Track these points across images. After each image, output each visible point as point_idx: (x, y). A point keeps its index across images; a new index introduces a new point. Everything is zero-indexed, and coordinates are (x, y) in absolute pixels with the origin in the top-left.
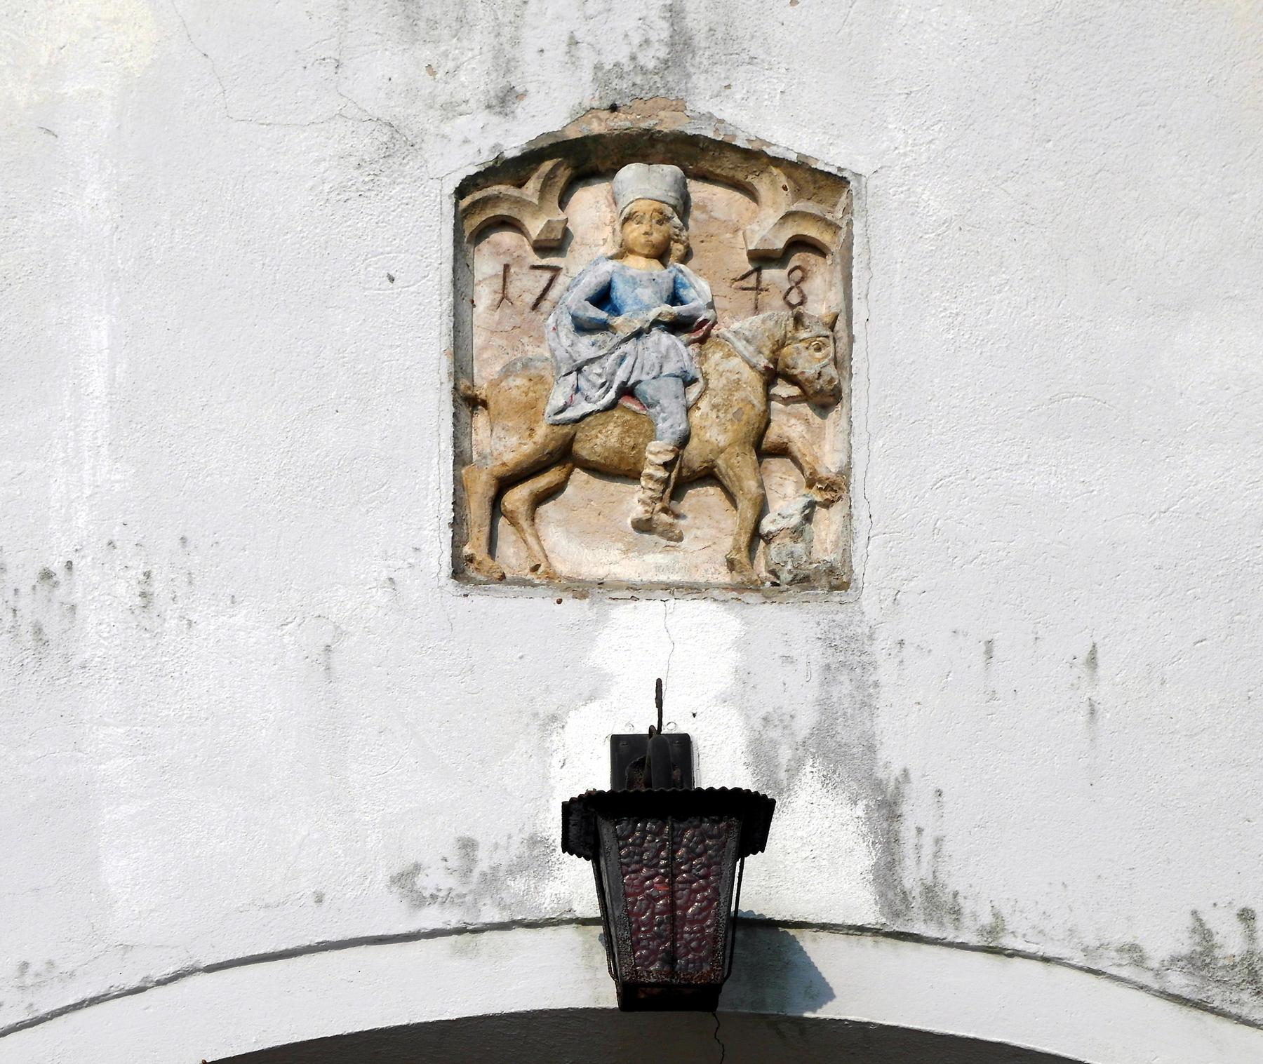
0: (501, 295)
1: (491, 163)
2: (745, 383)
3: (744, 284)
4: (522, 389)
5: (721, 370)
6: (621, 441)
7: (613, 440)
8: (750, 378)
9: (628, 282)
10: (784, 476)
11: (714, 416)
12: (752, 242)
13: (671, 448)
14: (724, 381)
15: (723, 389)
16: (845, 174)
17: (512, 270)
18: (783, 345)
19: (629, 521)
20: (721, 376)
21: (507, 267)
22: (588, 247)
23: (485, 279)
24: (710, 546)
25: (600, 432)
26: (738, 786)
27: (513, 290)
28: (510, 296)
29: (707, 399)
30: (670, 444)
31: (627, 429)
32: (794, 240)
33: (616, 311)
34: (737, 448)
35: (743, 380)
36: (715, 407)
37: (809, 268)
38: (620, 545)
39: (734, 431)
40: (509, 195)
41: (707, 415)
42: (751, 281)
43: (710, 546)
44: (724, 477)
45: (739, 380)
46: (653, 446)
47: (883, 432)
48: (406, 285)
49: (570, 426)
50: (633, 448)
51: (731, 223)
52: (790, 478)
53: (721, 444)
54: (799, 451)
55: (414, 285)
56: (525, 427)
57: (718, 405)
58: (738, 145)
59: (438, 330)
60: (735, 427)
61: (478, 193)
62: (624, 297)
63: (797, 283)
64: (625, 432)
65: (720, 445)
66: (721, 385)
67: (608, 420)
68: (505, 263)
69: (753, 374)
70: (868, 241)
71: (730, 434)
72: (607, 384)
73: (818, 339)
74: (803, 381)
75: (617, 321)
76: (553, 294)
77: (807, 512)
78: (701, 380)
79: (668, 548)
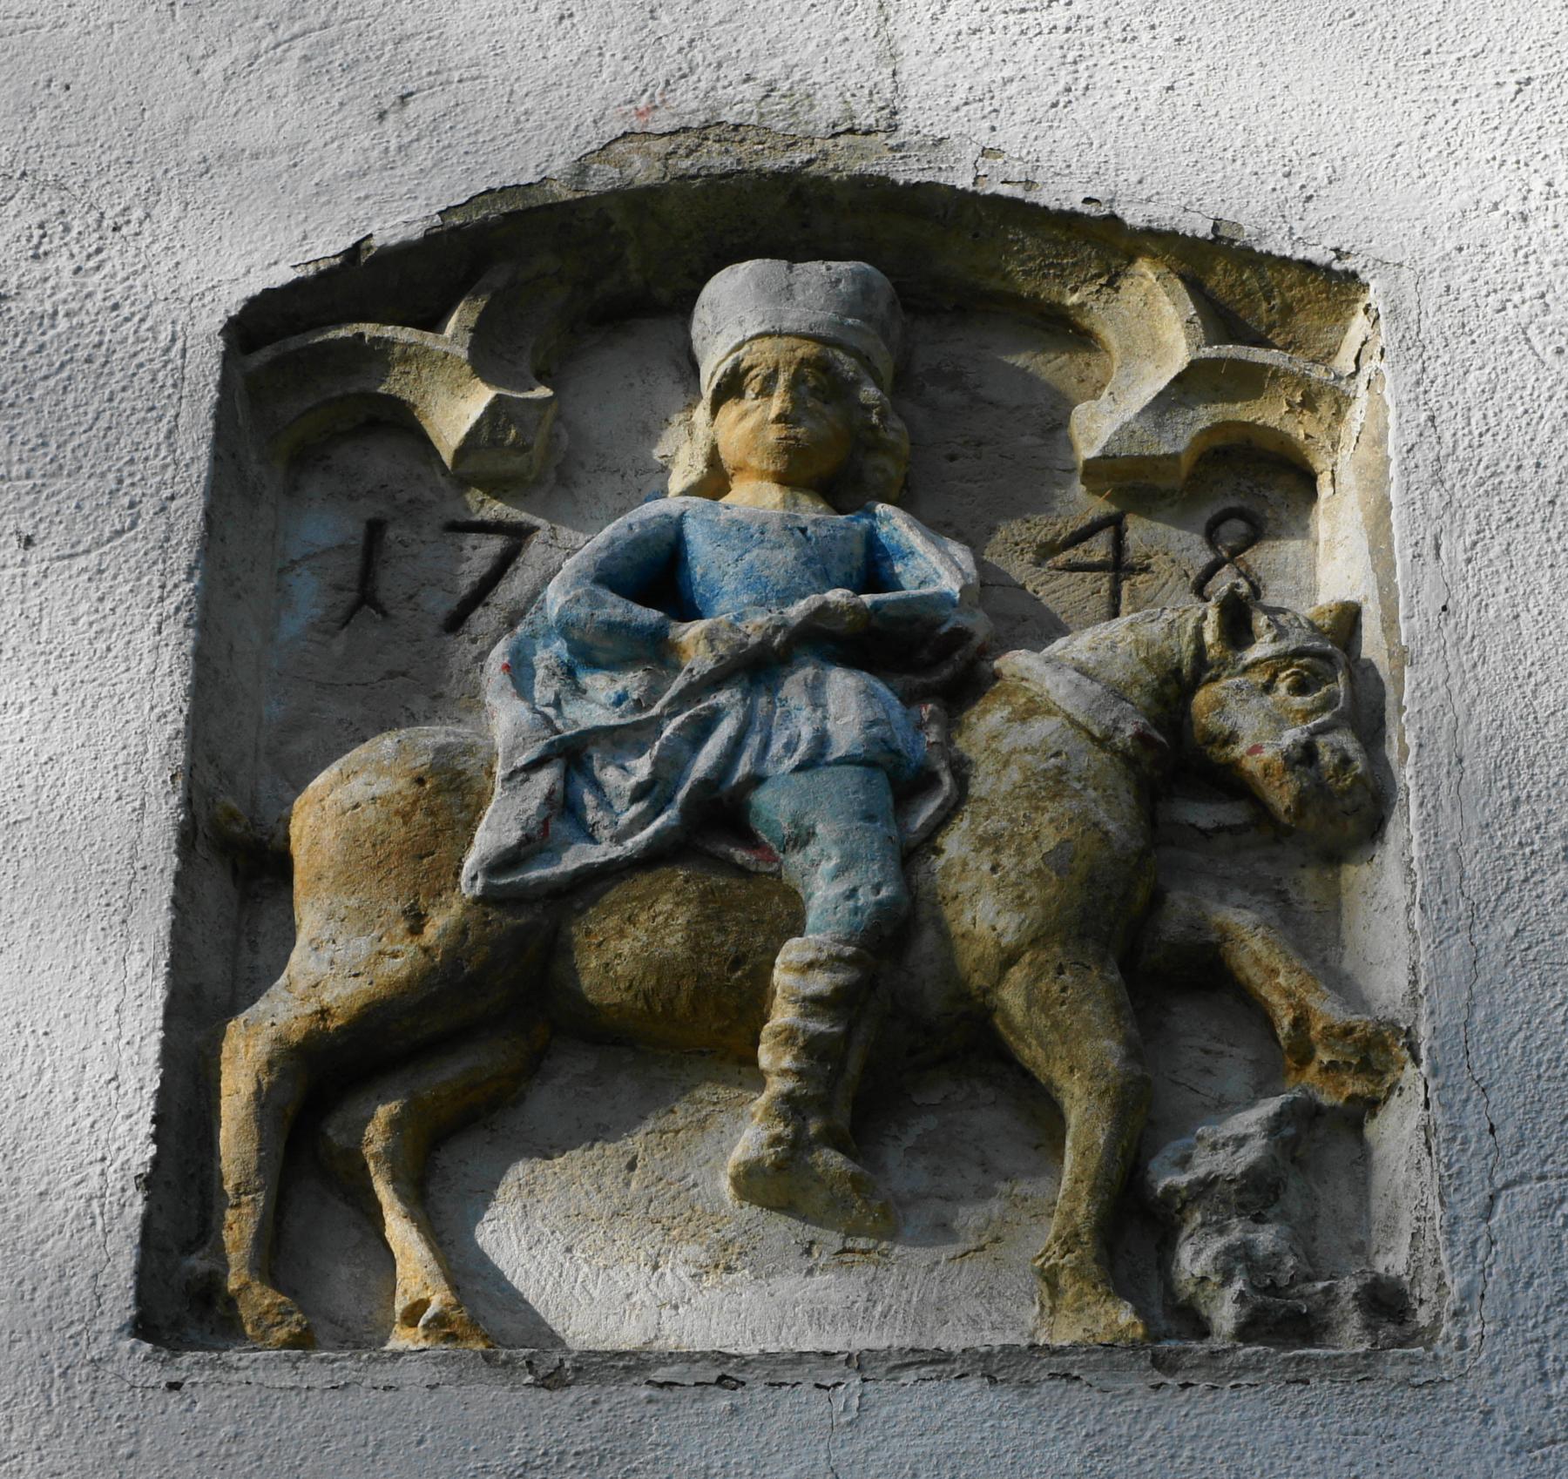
0: (353, 595)
1: (338, 260)
2: (1079, 779)
3: (1075, 554)
4: (394, 806)
5: (1005, 749)
6: (695, 942)
7: (670, 941)
8: (1096, 765)
9: (726, 536)
10: (1218, 1047)
11: (986, 867)
12: (1091, 443)
13: (849, 951)
14: (1014, 775)
15: (1011, 795)
16: (1349, 264)
17: (391, 534)
18: (1195, 684)
19: (725, 1184)
20: (1006, 764)
21: (375, 529)
22: (617, 477)
23: (306, 557)
24: (982, 1249)
25: (631, 920)
26: (255, 286)
27: (390, 585)
28: (381, 595)
29: (965, 824)
30: (847, 942)
31: (713, 910)
32: (1218, 441)
33: (687, 610)
34: (1057, 949)
35: (1074, 770)
36: (992, 842)
37: (1268, 513)
38: (690, 1250)
39: (1046, 904)
40: (387, 341)
41: (965, 864)
42: (1099, 549)
43: (982, 1249)
44: (1021, 1038)
45: (1061, 771)
46: (793, 951)
47: (1514, 895)
48: (67, 551)
49: (538, 909)
50: (737, 963)
51: (1034, 412)
52: (1235, 1051)
53: (1008, 939)
54: (1257, 961)
55: (87, 552)
56: (395, 908)
57: (997, 836)
58: (1042, 202)
59: (148, 661)
60: (1050, 891)
61: (296, 338)
62: (714, 574)
63: (1235, 552)
64: (708, 918)
65: (1004, 942)
66: (1005, 787)
67: (658, 886)
68: (371, 515)
69: (1104, 756)
70: (1432, 419)
71: (1035, 910)
72: (657, 789)
73: (1296, 662)
74: (1259, 774)
75: (689, 633)
76: (513, 588)
77: (1289, 1131)
78: (946, 779)
79: (848, 1257)
